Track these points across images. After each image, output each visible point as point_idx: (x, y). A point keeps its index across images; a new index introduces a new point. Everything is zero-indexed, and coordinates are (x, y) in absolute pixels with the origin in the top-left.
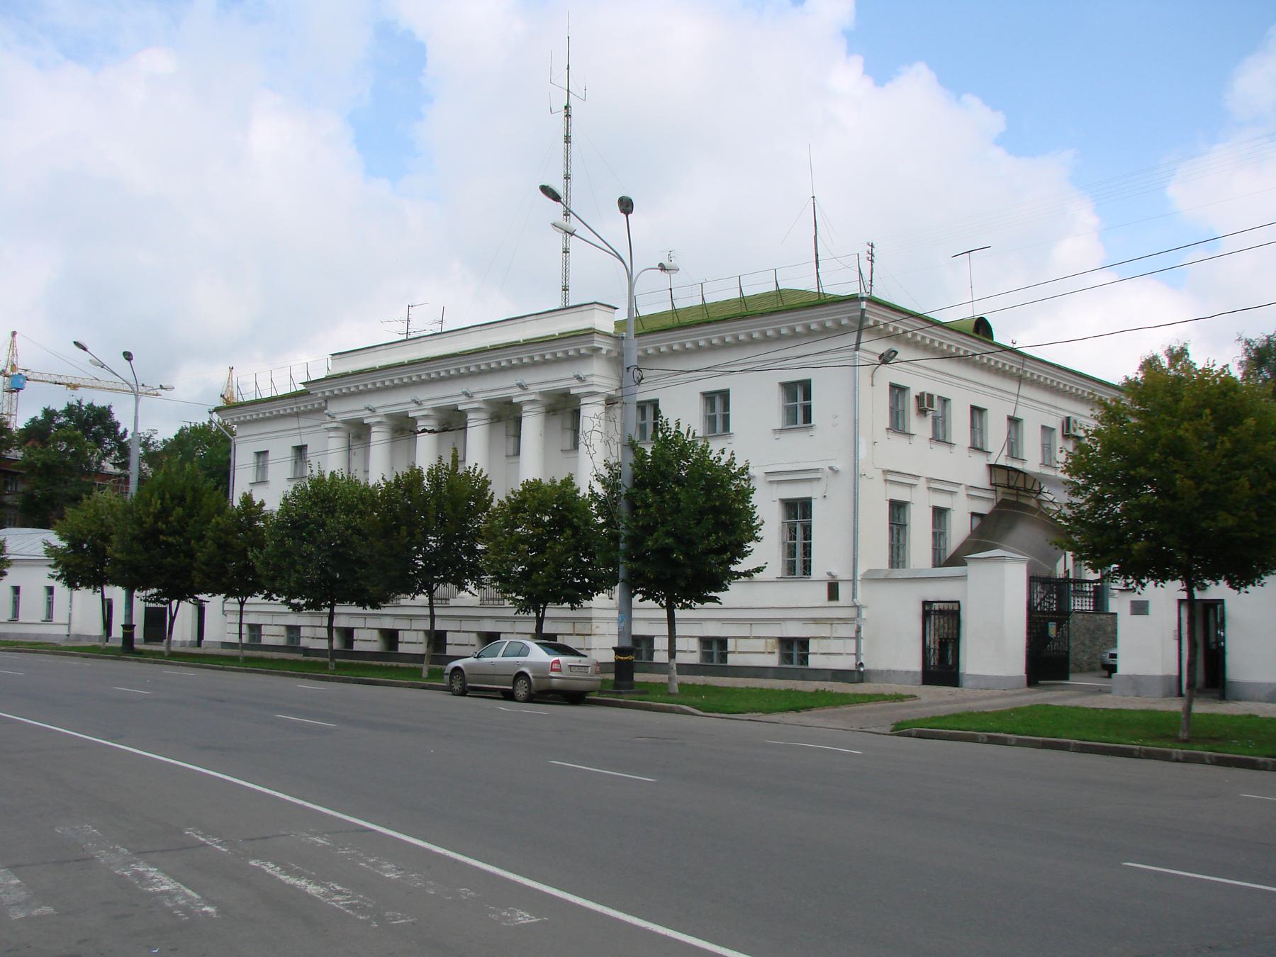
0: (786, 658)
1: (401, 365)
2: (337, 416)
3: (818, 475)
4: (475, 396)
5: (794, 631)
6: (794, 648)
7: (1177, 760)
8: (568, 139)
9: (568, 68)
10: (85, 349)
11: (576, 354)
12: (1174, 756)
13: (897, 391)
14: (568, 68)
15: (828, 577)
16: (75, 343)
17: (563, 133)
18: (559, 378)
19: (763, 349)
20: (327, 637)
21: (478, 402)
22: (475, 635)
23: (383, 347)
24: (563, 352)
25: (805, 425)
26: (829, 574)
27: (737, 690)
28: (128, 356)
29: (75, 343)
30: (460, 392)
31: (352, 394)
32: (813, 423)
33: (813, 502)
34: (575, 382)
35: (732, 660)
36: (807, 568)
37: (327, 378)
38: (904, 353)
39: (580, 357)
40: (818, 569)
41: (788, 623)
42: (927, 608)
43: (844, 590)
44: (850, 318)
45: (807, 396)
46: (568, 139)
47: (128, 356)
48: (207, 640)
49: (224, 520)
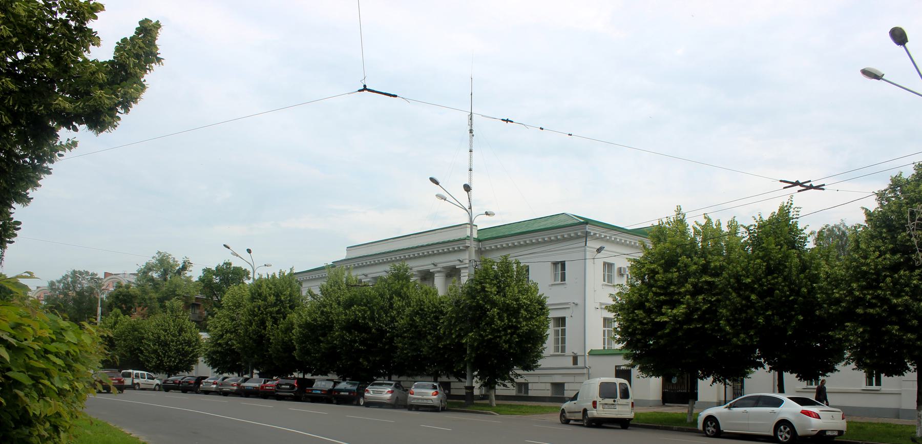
0: (520, 390)
1: (422, 246)
2: (369, 275)
3: (567, 306)
4: (438, 265)
5: (558, 379)
6: (559, 387)
7: (675, 430)
8: (471, 131)
9: (471, 95)
10: (229, 248)
11: (433, 253)
12: (674, 429)
13: (608, 266)
14: (471, 95)
15: (573, 354)
16: (224, 245)
17: (469, 128)
18: (450, 260)
19: (523, 249)
20: (827, 394)
21: (440, 268)
22: (550, 384)
23: (371, 245)
24: (458, 247)
25: (562, 282)
26: (573, 353)
27: (309, 400)
28: (249, 251)
29: (224, 245)
30: (430, 263)
31: (425, 256)
32: (566, 282)
33: (566, 318)
34: (458, 263)
35: (531, 393)
36: (563, 350)
37: (345, 260)
38: (608, 247)
39: (460, 250)
40: (569, 350)
41: (556, 376)
42: (617, 369)
43: (580, 360)
44: (581, 232)
45: (563, 268)
46: (471, 131)
47: (249, 251)
48: (701, 400)
49: (802, 276)
